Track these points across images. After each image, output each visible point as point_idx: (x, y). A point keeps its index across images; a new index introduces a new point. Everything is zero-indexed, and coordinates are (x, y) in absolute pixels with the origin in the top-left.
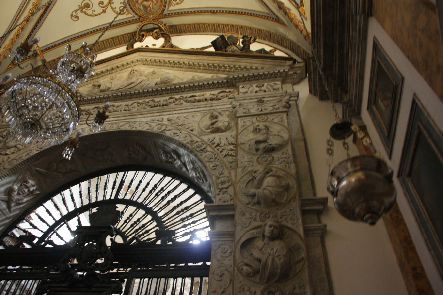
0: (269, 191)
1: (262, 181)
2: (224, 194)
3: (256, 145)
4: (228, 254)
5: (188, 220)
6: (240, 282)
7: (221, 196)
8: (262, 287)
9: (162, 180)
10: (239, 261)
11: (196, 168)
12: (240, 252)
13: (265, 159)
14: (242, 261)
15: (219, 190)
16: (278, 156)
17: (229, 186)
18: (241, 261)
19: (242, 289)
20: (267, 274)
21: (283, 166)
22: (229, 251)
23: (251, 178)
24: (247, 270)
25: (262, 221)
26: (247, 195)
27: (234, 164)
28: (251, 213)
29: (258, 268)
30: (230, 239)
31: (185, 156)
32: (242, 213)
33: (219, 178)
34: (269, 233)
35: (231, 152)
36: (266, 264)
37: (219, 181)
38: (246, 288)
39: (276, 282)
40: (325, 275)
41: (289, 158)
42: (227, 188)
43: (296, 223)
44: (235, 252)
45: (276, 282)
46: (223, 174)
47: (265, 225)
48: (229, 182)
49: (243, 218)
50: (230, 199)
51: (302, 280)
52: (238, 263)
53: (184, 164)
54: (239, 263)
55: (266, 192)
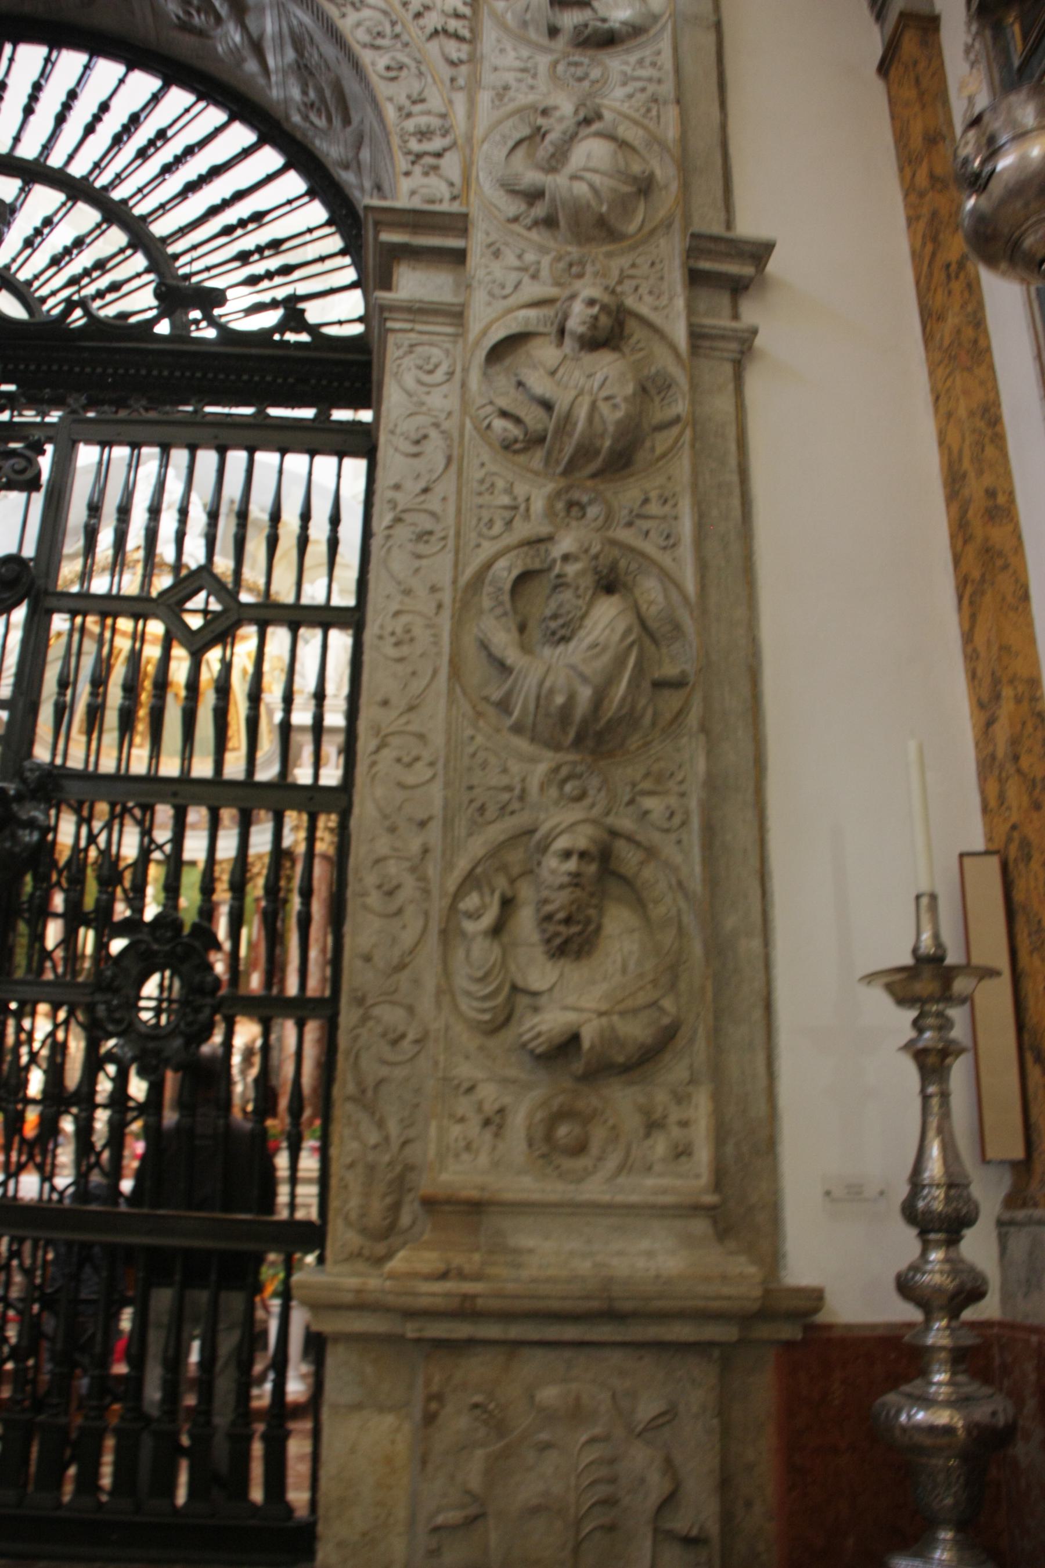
0: (592, 186)
1: (568, 150)
2: (426, 174)
3: (549, 10)
4: (439, 376)
5: (262, 258)
6: (483, 465)
7: (417, 179)
8: (550, 487)
9: (156, 98)
10: (480, 401)
11: (306, 66)
12: (485, 374)
13: (580, 71)
14: (491, 403)
15: (411, 158)
16: (625, 68)
17: (445, 150)
18: (484, 401)
19: (487, 485)
20: (569, 450)
21: (638, 110)
22: (444, 368)
23: (526, 131)
24: (505, 430)
25: (558, 284)
26: (512, 191)
27: (464, 69)
28: (523, 252)
29: (540, 427)
30: (449, 330)
31: (268, 13)
32: (493, 249)
33: (409, 115)
34: (584, 323)
35: (453, 24)
36: (568, 418)
37: (410, 125)
38: (500, 484)
39: (593, 476)
40: (735, 478)
41: (659, 81)
42: (439, 155)
43: (664, 307)
44: (465, 370)
45: (593, 476)
46: (423, 101)
47: (573, 297)
48: (444, 136)
49: (496, 268)
50: (447, 196)
51: (669, 478)
52: (477, 405)
53: (257, 48)
54: (478, 409)
55: (581, 189)
